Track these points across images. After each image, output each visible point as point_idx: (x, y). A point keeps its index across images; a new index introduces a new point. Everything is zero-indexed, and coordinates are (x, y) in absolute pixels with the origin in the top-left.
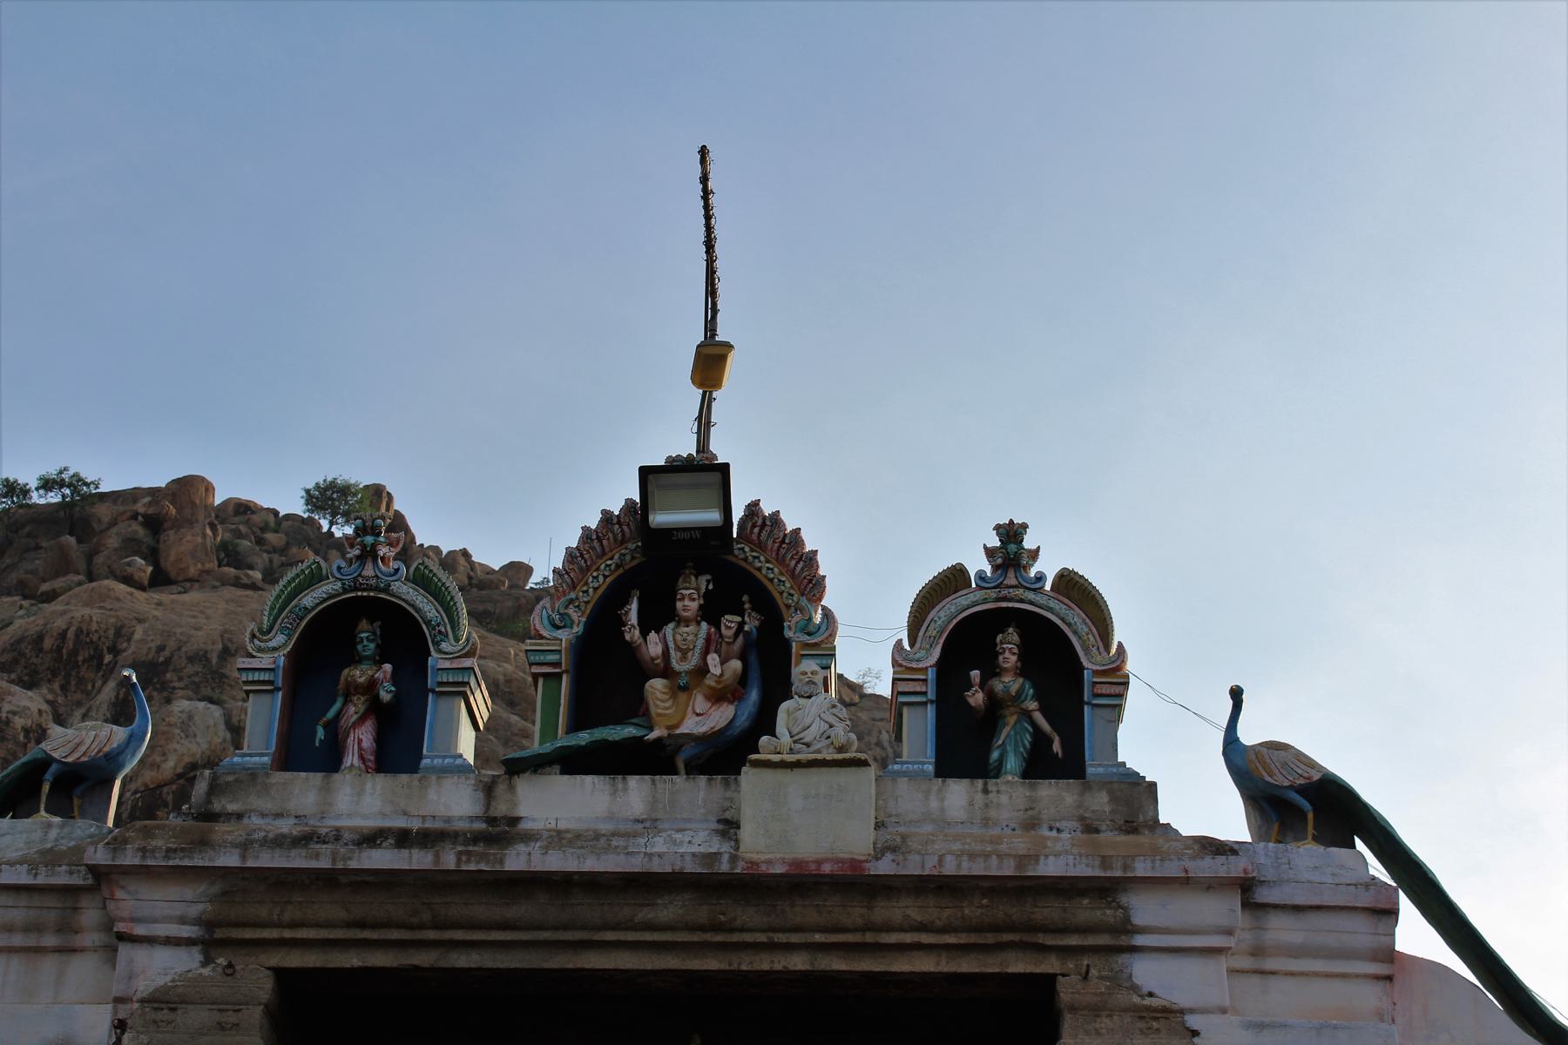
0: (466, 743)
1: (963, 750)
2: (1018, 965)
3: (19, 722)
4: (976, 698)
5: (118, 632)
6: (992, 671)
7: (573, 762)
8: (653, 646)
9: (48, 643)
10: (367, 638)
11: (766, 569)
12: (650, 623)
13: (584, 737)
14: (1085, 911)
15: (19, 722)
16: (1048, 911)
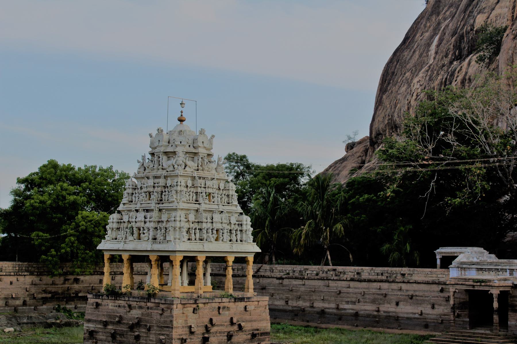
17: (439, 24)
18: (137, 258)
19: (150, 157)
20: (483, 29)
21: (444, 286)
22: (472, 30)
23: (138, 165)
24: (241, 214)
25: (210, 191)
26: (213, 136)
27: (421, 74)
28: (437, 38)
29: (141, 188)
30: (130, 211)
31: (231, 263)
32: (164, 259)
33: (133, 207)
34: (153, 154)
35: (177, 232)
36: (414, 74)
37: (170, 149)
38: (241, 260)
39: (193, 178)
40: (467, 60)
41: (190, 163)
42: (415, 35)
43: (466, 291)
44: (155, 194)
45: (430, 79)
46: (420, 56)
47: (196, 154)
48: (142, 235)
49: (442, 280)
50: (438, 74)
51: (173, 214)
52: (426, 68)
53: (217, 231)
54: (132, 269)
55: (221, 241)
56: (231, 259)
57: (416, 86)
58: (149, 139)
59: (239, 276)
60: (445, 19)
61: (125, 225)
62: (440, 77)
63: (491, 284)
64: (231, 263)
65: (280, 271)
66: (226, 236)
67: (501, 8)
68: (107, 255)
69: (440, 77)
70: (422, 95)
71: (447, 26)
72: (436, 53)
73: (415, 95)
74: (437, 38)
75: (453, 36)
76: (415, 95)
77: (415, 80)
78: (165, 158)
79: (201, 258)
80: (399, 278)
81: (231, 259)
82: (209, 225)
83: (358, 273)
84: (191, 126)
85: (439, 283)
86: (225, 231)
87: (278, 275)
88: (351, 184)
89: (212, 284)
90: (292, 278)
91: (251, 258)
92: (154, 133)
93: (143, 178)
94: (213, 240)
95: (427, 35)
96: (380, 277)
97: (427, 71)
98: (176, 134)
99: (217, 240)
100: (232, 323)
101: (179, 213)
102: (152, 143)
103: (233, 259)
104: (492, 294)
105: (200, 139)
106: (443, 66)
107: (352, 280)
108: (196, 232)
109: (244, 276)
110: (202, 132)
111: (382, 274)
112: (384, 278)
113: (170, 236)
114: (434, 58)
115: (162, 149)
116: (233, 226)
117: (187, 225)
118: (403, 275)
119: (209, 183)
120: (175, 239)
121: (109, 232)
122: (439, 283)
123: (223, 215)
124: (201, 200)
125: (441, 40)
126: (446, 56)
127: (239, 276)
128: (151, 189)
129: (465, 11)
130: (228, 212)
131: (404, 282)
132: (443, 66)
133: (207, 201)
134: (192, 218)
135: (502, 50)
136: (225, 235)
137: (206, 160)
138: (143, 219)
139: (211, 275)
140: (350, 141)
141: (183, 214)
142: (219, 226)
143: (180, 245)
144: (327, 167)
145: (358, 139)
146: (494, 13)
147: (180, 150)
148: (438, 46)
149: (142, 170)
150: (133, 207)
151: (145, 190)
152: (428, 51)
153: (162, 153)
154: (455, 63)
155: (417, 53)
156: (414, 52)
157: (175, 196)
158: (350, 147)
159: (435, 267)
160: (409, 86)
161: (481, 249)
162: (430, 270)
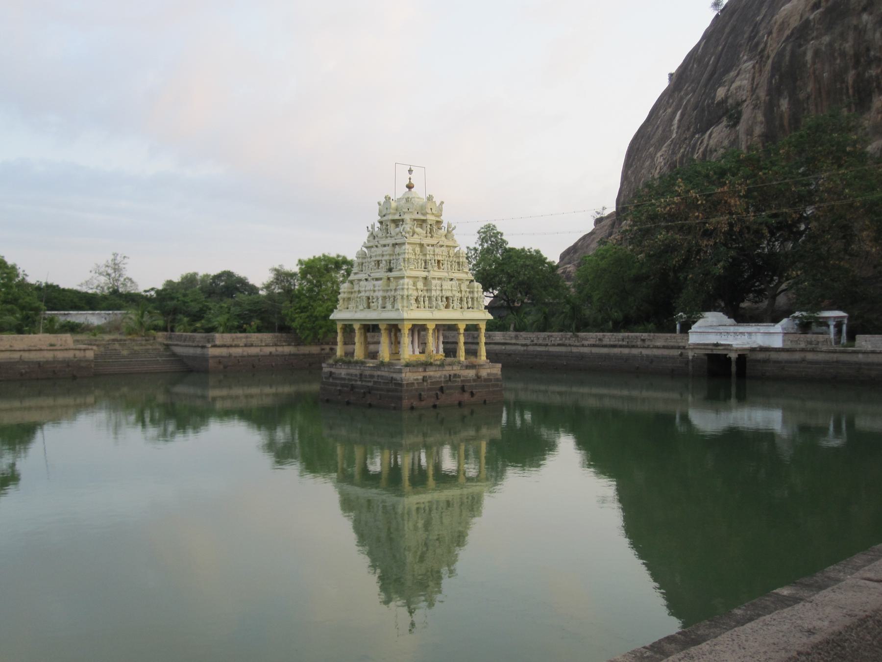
17: (681, 99)
18: (371, 328)
19: (379, 225)
20: (724, 101)
21: (683, 351)
22: (713, 103)
23: (368, 234)
24: (472, 281)
25: (440, 258)
26: (442, 203)
27: (664, 149)
28: (679, 112)
29: (371, 257)
30: (360, 280)
31: (462, 331)
32: (394, 328)
33: (362, 276)
34: (381, 223)
35: (405, 301)
36: (658, 149)
37: (397, 217)
38: (472, 328)
39: (421, 245)
40: (708, 133)
41: (418, 230)
42: (658, 112)
43: (708, 355)
44: (384, 262)
45: (674, 153)
46: (664, 131)
47: (424, 221)
48: (372, 304)
49: (681, 344)
50: (680, 148)
51: (401, 281)
52: (669, 142)
53: (447, 298)
54: (366, 338)
55: (451, 309)
56: (462, 327)
57: (660, 159)
58: (378, 207)
59: (472, 343)
60: (687, 94)
61: (356, 295)
62: (682, 150)
63: (369, 456)
64: (462, 331)
65: (525, 339)
66: (456, 304)
67: (741, 80)
68: (339, 326)
69: (682, 150)
70: (665, 168)
71: (689, 101)
72: (678, 127)
73: (658, 168)
74: (679, 112)
75: (694, 110)
76: (658, 168)
77: (659, 154)
78: (393, 225)
79: (431, 326)
80: (639, 343)
81: (462, 327)
82: (438, 293)
83: (600, 340)
84: (420, 193)
85: (679, 348)
86: (455, 299)
87: (524, 342)
88: (596, 255)
89: (444, 351)
90: (536, 345)
91: (483, 326)
92: (383, 200)
93: (372, 247)
94: (442, 307)
95: (669, 110)
96: (620, 343)
97: (670, 145)
98: (404, 200)
99: (447, 307)
100: (463, 389)
101: (406, 280)
102: (380, 211)
103: (464, 327)
104: (730, 358)
105: (429, 206)
106: (686, 139)
107: (594, 346)
108: (425, 300)
109: (478, 344)
110: (430, 198)
111: (623, 340)
112: (624, 343)
113: (399, 305)
114: (677, 133)
115: (390, 217)
116: (463, 293)
117: (415, 294)
118: (643, 340)
119: (438, 250)
120: (403, 307)
121: (341, 302)
122: (679, 348)
123: (453, 282)
124: (430, 268)
125: (682, 115)
126: (689, 129)
127: (472, 343)
128: (379, 258)
129: (706, 85)
130: (458, 280)
131: (644, 347)
132: (686, 139)
133: (436, 268)
134: (420, 285)
135: (742, 121)
136: (455, 302)
137: (435, 227)
138: (372, 288)
139: (443, 343)
140: (598, 216)
141: (411, 282)
142: (449, 294)
143: (413, 313)
144: (576, 240)
145: (606, 213)
146: (734, 86)
147: (407, 217)
148: (680, 121)
149: (371, 238)
150: (362, 276)
151: (374, 259)
152: (671, 125)
153: (392, 220)
154: (697, 136)
155: (660, 129)
156: (658, 127)
157: (402, 264)
158: (598, 221)
159: (674, 331)
160: (653, 160)
161: (721, 314)
162: (669, 335)
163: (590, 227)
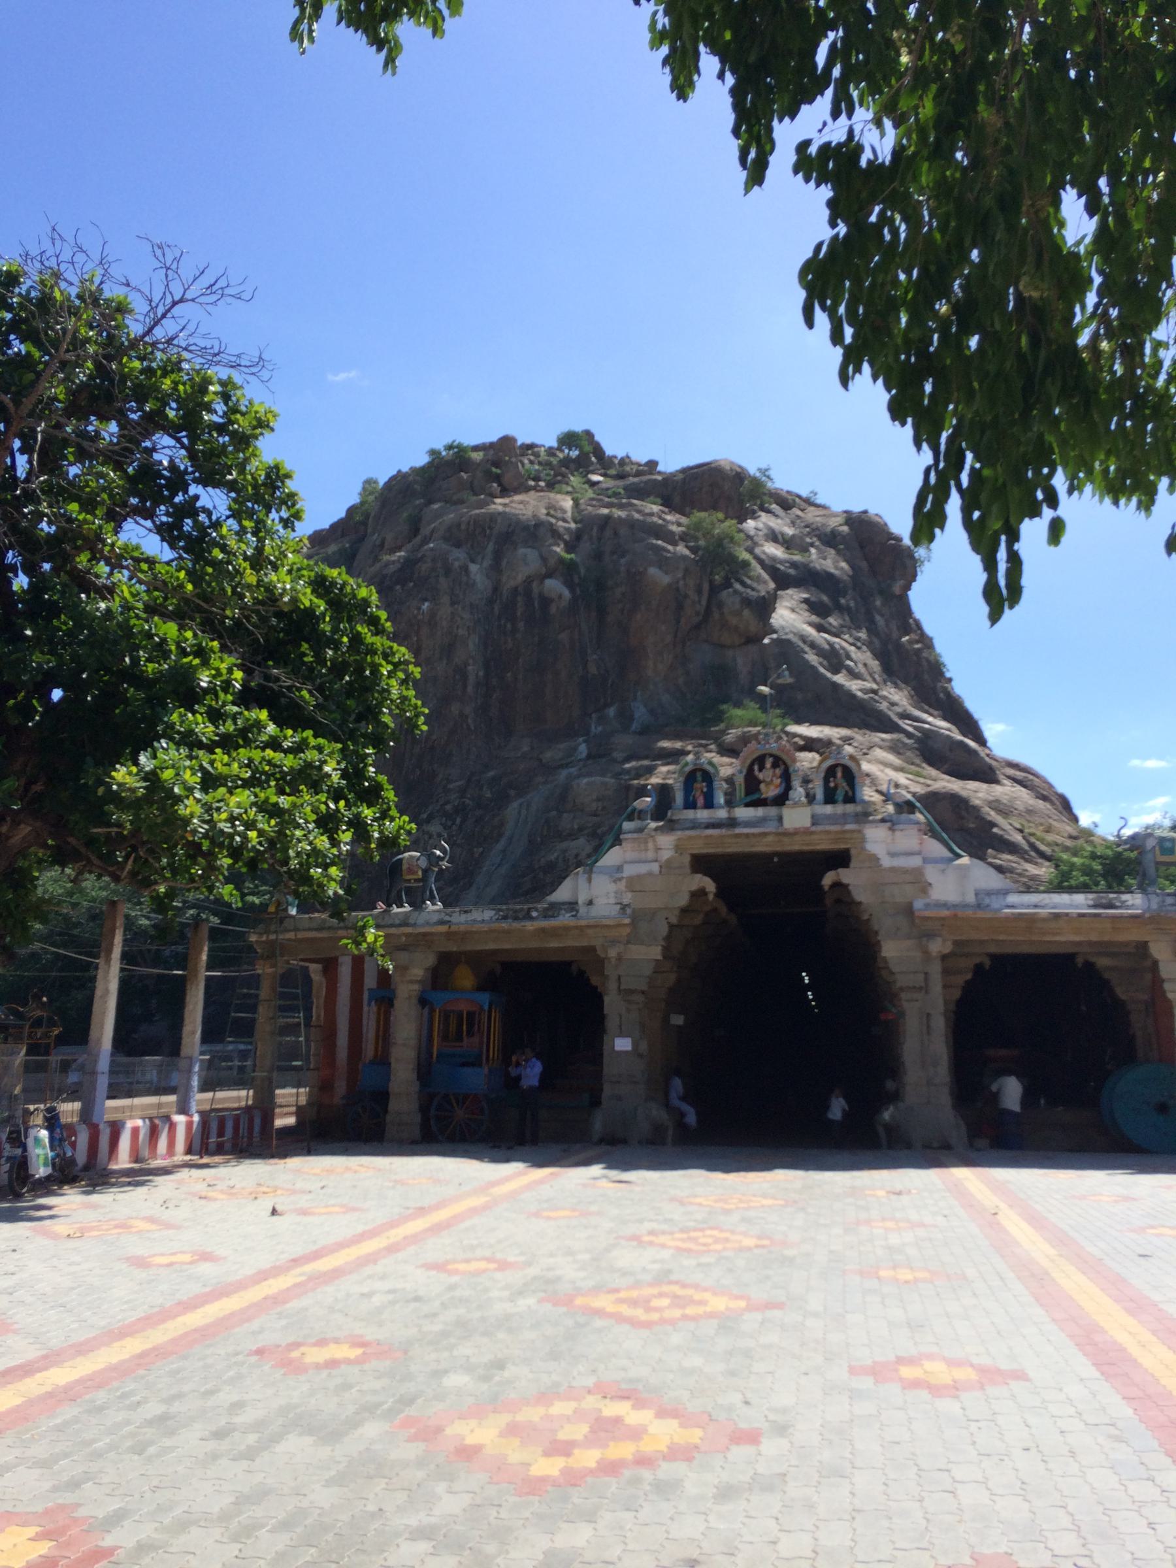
0: (722, 801)
1: (830, 799)
2: (843, 846)
3: (457, 564)
4: (832, 785)
5: (491, 520)
6: (835, 777)
7: (747, 805)
8: (761, 776)
9: (463, 527)
10: (699, 775)
11: (784, 757)
12: (760, 770)
13: (749, 799)
14: (855, 835)
15: (457, 564)
16: (848, 836)
163: (422, 460)
